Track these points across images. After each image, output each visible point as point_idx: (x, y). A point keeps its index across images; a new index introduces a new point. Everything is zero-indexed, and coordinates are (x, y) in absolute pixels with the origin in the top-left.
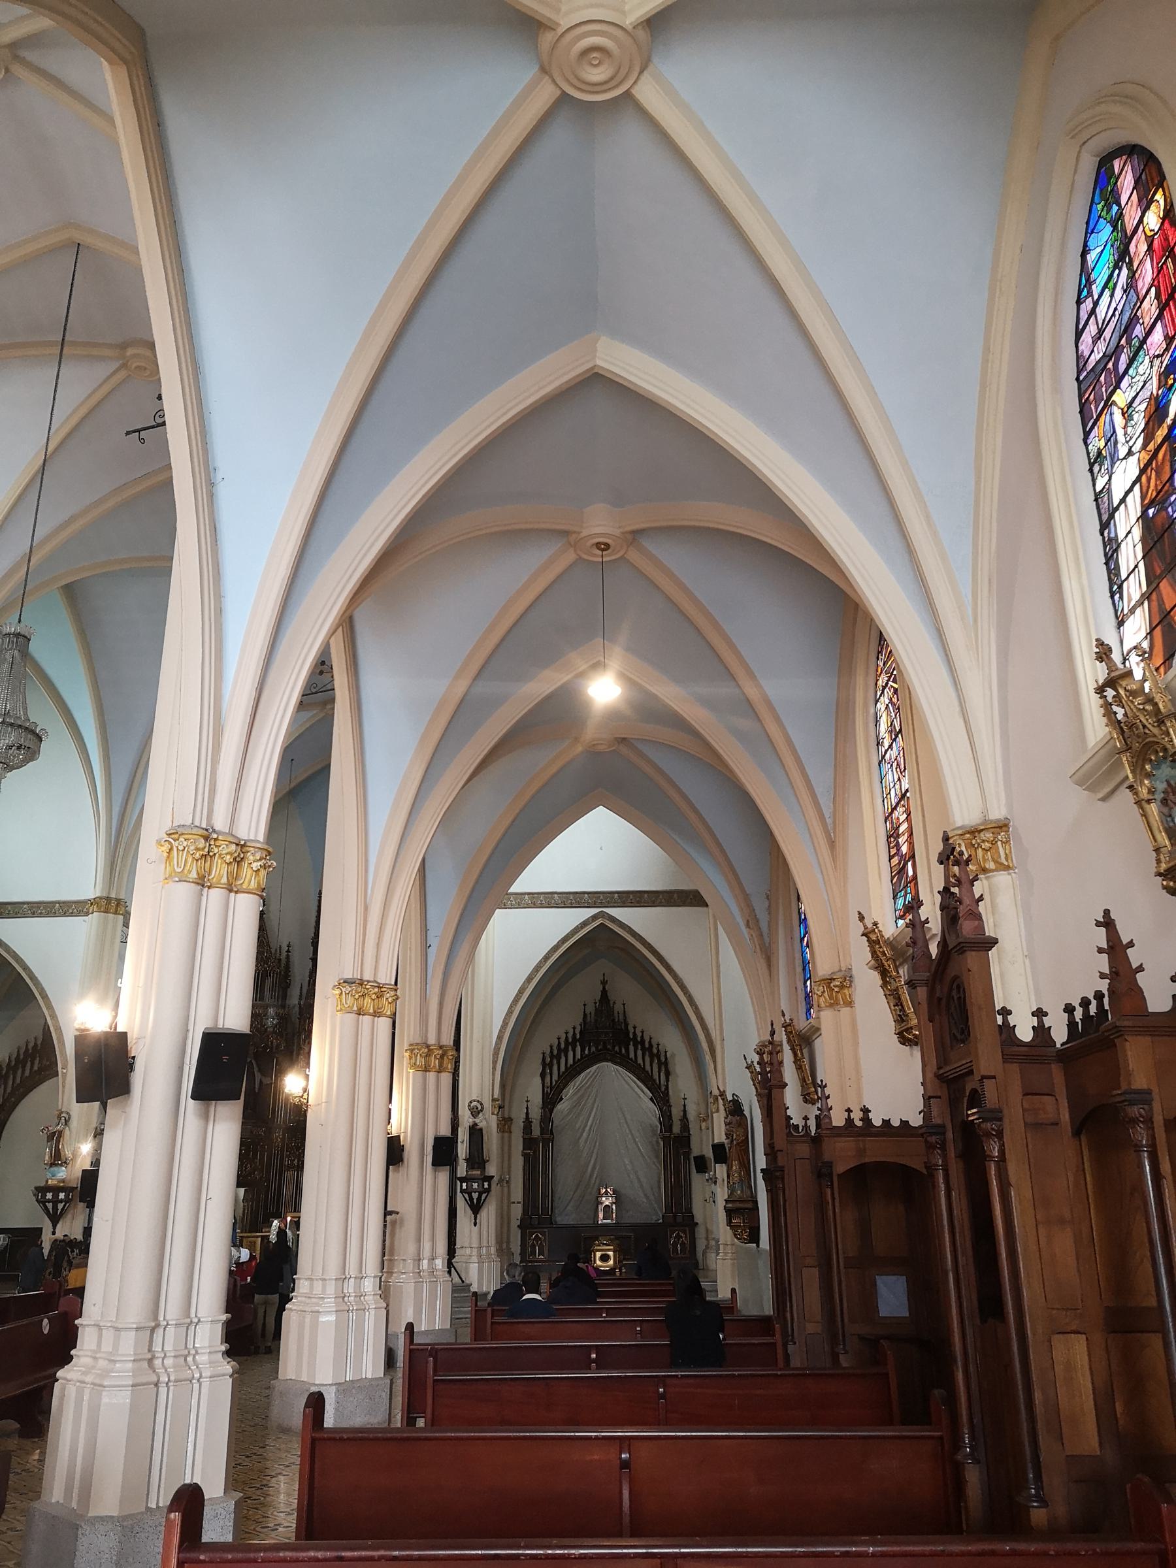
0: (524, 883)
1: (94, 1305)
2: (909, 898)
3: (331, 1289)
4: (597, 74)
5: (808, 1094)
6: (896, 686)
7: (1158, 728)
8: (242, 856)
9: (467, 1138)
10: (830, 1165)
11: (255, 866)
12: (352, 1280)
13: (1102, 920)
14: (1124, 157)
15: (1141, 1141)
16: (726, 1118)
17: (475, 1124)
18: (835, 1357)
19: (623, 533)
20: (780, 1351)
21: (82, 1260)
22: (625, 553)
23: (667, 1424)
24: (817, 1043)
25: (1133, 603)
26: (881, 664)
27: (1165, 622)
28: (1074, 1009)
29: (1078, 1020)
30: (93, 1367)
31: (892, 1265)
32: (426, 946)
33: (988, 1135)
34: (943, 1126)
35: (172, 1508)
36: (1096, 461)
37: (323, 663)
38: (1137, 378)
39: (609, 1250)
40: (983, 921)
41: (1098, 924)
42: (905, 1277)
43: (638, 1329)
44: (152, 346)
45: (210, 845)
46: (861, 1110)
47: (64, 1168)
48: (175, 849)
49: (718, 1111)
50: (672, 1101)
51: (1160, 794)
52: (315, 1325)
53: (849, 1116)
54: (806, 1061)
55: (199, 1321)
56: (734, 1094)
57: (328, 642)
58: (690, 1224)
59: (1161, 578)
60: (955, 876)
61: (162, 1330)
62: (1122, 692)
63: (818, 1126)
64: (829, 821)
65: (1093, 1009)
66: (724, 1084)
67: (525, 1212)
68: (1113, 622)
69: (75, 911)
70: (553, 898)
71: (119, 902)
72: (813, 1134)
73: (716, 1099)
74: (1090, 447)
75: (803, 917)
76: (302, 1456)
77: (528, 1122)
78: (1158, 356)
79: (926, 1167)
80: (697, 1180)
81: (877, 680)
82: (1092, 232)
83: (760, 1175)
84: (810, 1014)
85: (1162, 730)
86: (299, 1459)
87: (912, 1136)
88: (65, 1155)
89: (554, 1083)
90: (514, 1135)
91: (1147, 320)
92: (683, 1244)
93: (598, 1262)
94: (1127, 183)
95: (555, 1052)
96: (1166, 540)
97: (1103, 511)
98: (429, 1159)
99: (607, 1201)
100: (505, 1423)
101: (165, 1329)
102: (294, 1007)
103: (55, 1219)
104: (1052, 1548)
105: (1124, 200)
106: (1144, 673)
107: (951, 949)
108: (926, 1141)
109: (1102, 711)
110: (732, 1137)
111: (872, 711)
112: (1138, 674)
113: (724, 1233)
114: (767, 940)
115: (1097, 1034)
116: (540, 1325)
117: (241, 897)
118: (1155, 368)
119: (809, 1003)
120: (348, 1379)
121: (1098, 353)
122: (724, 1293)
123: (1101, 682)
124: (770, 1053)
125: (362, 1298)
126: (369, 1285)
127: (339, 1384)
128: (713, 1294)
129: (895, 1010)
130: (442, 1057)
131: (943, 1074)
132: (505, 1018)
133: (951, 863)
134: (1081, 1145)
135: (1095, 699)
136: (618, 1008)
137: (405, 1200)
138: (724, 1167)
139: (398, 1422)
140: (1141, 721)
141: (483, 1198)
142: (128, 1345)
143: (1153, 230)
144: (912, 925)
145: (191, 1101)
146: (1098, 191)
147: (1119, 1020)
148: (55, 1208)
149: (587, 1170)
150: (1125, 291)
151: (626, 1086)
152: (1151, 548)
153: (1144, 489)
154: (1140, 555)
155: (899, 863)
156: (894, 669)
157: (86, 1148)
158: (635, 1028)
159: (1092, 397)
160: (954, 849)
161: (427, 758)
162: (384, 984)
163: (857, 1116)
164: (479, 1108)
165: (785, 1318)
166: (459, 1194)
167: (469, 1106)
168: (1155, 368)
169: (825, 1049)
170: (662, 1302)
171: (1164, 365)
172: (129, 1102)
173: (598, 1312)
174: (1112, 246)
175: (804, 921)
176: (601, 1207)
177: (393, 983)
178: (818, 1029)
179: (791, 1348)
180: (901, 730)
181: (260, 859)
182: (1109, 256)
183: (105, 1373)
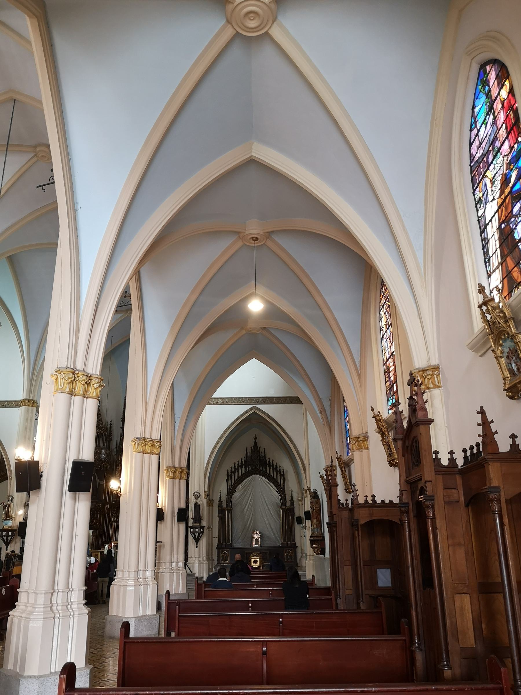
0: (218, 394)
1: (26, 582)
2: (394, 400)
3: (132, 575)
4: (252, 24)
5: (348, 489)
6: (389, 304)
7: (505, 324)
8: (89, 381)
9: (193, 509)
10: (357, 520)
11: (96, 386)
12: (142, 572)
13: (480, 411)
14: (491, 65)
15: (495, 509)
16: (310, 500)
17: (197, 503)
18: (358, 604)
19: (264, 233)
20: (334, 603)
21: (19, 563)
22: (266, 242)
23: (284, 635)
24: (352, 466)
25: (495, 267)
26: (382, 293)
27: (509, 276)
28: (467, 451)
29: (468, 455)
30: (26, 610)
31: (384, 564)
32: (174, 422)
33: (428, 507)
34: (408, 503)
35: (62, 673)
36: (479, 202)
37: (126, 292)
38: (497, 165)
39: (257, 558)
40: (427, 411)
41: (478, 413)
42: (389, 570)
43: (271, 593)
44: (48, 146)
45: (75, 376)
46: (372, 496)
47: (11, 521)
48: (59, 378)
49: (307, 497)
50: (286, 492)
51: (506, 354)
52: (125, 591)
53: (366, 499)
54: (347, 474)
55: (73, 589)
56: (314, 489)
57: (129, 283)
58: (294, 547)
59: (507, 256)
60: (415, 391)
61: (56, 594)
62: (490, 307)
63: (352, 503)
64: (358, 365)
65: (475, 451)
66: (310, 485)
67: (219, 541)
68: (486, 276)
69: (14, 405)
70: (232, 400)
71: (34, 401)
72: (350, 507)
73: (306, 491)
74: (476, 196)
75: (346, 409)
76: (120, 649)
77: (221, 502)
78: (506, 155)
79: (400, 521)
80: (297, 527)
81: (381, 301)
82: (477, 99)
83: (326, 525)
84: (349, 453)
85: (507, 325)
86: (119, 650)
87: (395, 507)
88: (11, 515)
89: (232, 484)
90: (214, 508)
91: (501, 139)
92: (291, 556)
93: (253, 564)
94: (492, 76)
95: (233, 470)
96: (509, 238)
97: (481, 225)
98: (176, 518)
99: (256, 537)
100: (211, 635)
101: (57, 593)
102: (114, 449)
103: (7, 544)
104: (453, 687)
105: (491, 84)
106: (500, 299)
107: (413, 424)
108: (400, 510)
109: (481, 316)
110: (313, 508)
111: (378, 315)
112: (497, 300)
113: (309, 550)
114: (329, 419)
115: (477, 462)
116: (227, 591)
117: (89, 400)
118: (505, 161)
119: (349, 448)
120: (140, 615)
121: (480, 153)
122: (309, 577)
123: (480, 303)
124: (331, 471)
125: (146, 579)
126: (149, 574)
127: (136, 617)
128: (304, 577)
129: (387, 451)
130: (181, 472)
131: (408, 480)
132: (210, 455)
133: (413, 385)
134: (469, 511)
135: (478, 311)
136: (262, 450)
137: (165, 536)
138: (310, 521)
139: (163, 635)
140: (498, 321)
141: (200, 536)
142: (41, 600)
143: (504, 98)
144: (395, 413)
145: (68, 492)
146: (479, 80)
147: (486, 456)
148: (7, 539)
149: (248, 522)
150: (492, 126)
151: (266, 486)
152: (503, 242)
153: (500, 215)
154: (498, 245)
155: (390, 385)
156: (388, 296)
157: (21, 512)
158: (269, 459)
159: (477, 173)
160: (415, 379)
161: (174, 336)
162: (154, 440)
163: (370, 499)
164: (199, 496)
165: (336, 587)
166: (189, 534)
167: (194, 494)
168: (505, 161)
169: (355, 469)
170: (281, 581)
171: (509, 159)
172: (40, 492)
173: (252, 586)
174: (486, 105)
175: (346, 411)
176: (254, 540)
177: (159, 439)
178: (353, 460)
179: (339, 601)
180: (391, 324)
181: (98, 383)
182: (485, 110)
183: (31, 613)
